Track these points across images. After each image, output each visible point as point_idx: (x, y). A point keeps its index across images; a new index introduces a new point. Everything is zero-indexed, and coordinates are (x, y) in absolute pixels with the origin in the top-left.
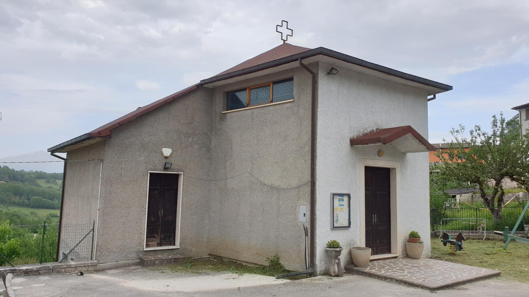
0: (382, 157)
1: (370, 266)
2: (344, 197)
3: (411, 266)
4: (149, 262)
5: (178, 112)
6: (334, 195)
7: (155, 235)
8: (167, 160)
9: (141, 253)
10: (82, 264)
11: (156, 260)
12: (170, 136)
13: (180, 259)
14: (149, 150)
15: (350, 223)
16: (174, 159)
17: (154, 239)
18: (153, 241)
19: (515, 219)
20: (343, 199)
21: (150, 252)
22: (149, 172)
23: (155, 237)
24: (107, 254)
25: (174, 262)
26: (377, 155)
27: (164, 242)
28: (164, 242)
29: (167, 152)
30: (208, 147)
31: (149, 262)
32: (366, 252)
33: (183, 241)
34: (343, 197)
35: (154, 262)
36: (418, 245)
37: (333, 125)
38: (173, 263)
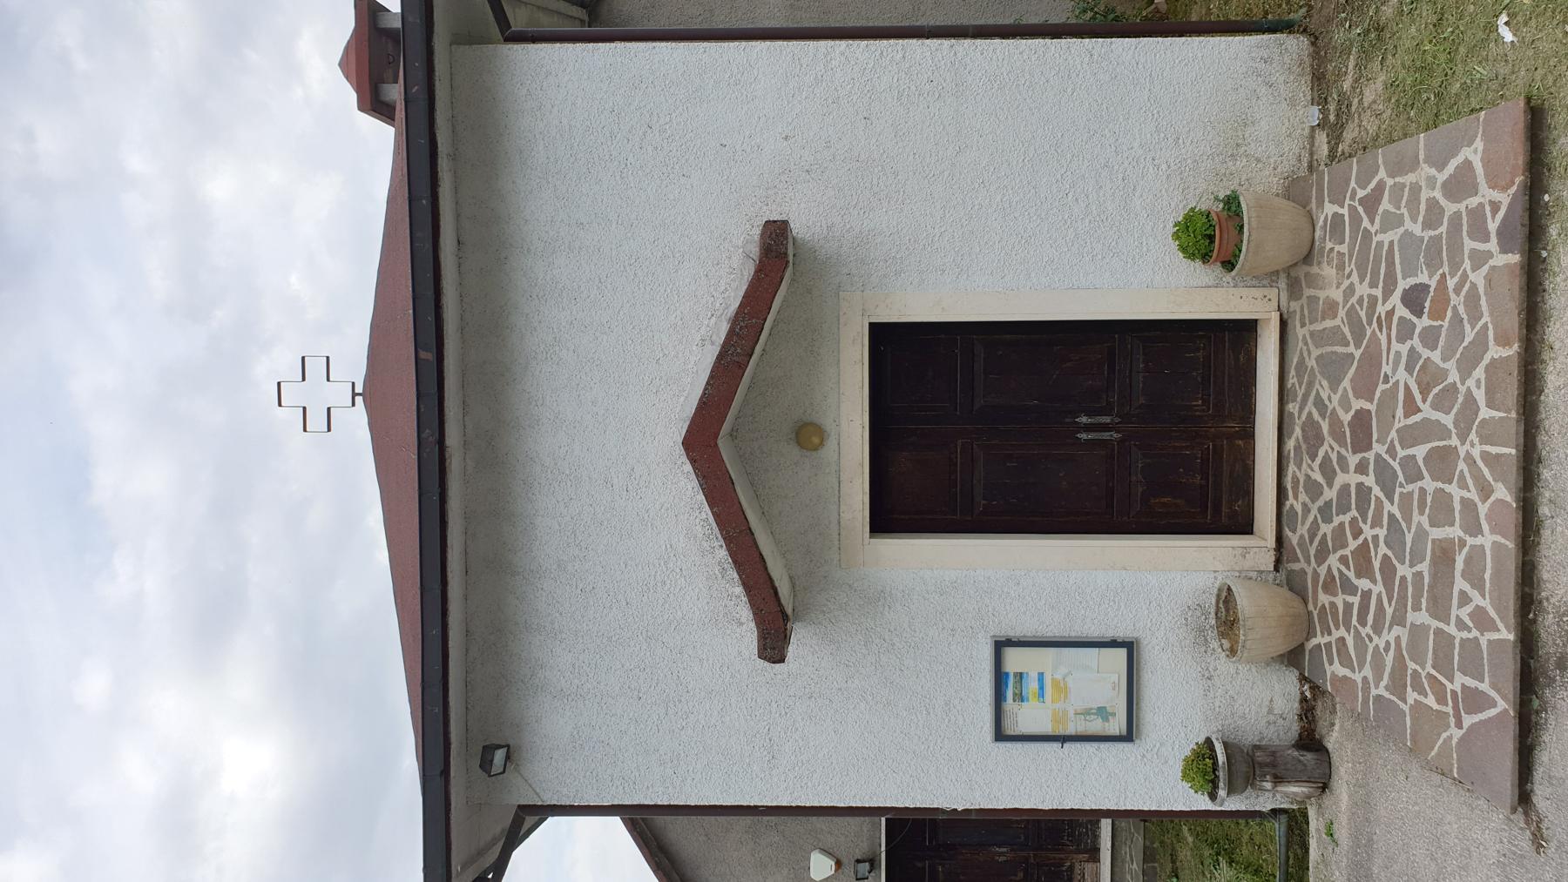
0: (828, 424)
1: (1297, 439)
2: (1007, 670)
5: (696, 834)
7: (1064, 869)
8: (845, 861)
12: (773, 856)
13: (1148, 843)
15: (1113, 644)
16: (843, 838)
17: (1077, 871)
18: (1084, 874)
19: (1304, 816)
20: (1016, 674)
23: (1071, 868)
25: (1154, 863)
27: (1089, 841)
28: (1089, 841)
32: (1248, 644)
34: (1007, 674)
36: (1254, 224)
37: (713, 721)
38: (1156, 865)
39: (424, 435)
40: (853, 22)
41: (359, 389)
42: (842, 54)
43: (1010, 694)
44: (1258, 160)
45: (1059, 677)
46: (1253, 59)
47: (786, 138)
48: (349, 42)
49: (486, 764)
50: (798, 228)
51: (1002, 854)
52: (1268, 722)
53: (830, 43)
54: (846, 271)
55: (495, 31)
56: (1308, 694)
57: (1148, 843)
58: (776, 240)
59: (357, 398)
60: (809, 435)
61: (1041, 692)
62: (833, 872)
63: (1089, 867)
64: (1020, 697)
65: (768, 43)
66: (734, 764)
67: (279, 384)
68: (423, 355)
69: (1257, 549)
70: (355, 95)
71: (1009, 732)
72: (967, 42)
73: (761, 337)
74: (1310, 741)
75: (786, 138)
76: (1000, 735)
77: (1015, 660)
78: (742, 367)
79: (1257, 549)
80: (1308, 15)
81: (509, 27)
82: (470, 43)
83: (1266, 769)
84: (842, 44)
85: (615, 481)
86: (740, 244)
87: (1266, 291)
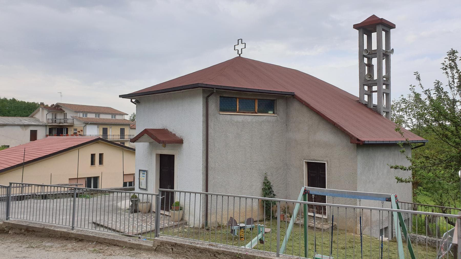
40: (210, 159)
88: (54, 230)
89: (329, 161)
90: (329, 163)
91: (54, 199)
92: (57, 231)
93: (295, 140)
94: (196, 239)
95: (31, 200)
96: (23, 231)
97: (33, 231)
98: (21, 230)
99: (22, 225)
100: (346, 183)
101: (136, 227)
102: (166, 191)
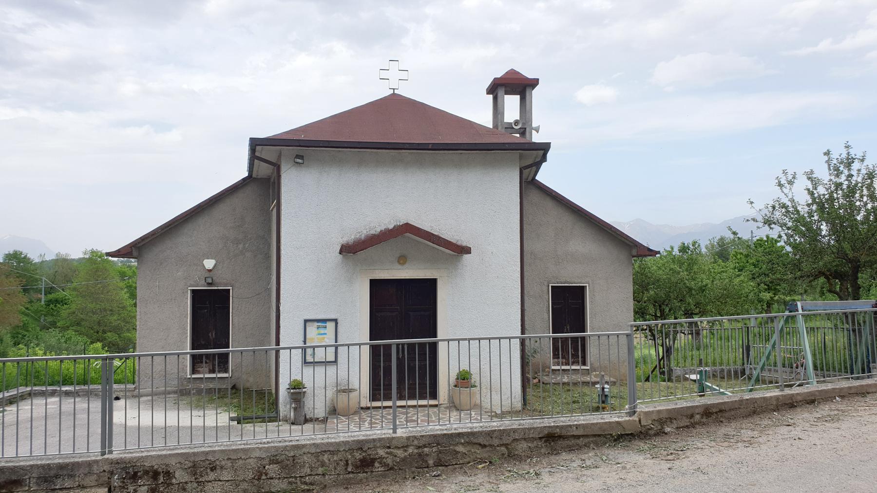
0: (406, 266)
3: (387, 423)
4: (184, 391)
6: (306, 321)
8: (211, 273)
9: (185, 380)
10: (118, 388)
11: (193, 389)
14: (188, 264)
20: (326, 326)
21: (195, 379)
22: (189, 288)
24: (146, 379)
26: (397, 263)
29: (209, 264)
30: (266, 254)
31: (184, 391)
33: (237, 368)
35: (190, 391)
39: (406, 144)
40: (526, 274)
41: (396, 92)
42: (516, 270)
43: (319, 324)
44: (486, 396)
45: (326, 339)
46: (515, 393)
47: (492, 253)
48: (519, 73)
49: (298, 157)
50: (466, 256)
51: (212, 335)
52: (309, 408)
53: (520, 266)
54: (453, 271)
55: (523, 165)
56: (320, 419)
57: (223, 390)
58: (467, 250)
59: (392, 90)
60: (402, 260)
61: (319, 334)
62: (207, 268)
63: (207, 370)
64: (318, 327)
65: (519, 248)
66: (296, 236)
67: (407, 71)
68: (431, 145)
69: (365, 402)
70: (499, 77)
71: (307, 324)
72: (520, 307)
73: (435, 245)
74: (306, 421)
75: (492, 253)
76: (306, 321)
77: (331, 326)
78: (430, 241)
79: (365, 402)
80: (528, 410)
81: (524, 169)
82: (520, 157)
83: (299, 405)
84: (519, 269)
85: (388, 199)
86: (461, 239)
87: (447, 400)
88: (764, 398)
89: (590, 283)
90: (591, 286)
91: (63, 398)
92: (771, 397)
93: (532, 253)
94: (586, 413)
95: (32, 401)
96: (698, 417)
97: (721, 411)
98: (692, 416)
99: (692, 407)
100: (618, 313)
101: (447, 414)
102: (218, 354)
